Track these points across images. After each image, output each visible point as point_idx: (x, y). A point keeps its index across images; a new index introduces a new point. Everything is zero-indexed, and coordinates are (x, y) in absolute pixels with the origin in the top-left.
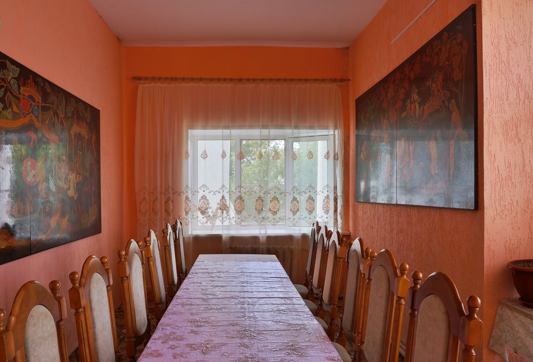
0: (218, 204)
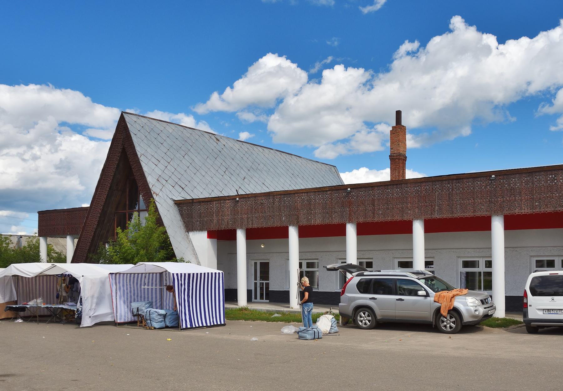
0: (22, 241)
